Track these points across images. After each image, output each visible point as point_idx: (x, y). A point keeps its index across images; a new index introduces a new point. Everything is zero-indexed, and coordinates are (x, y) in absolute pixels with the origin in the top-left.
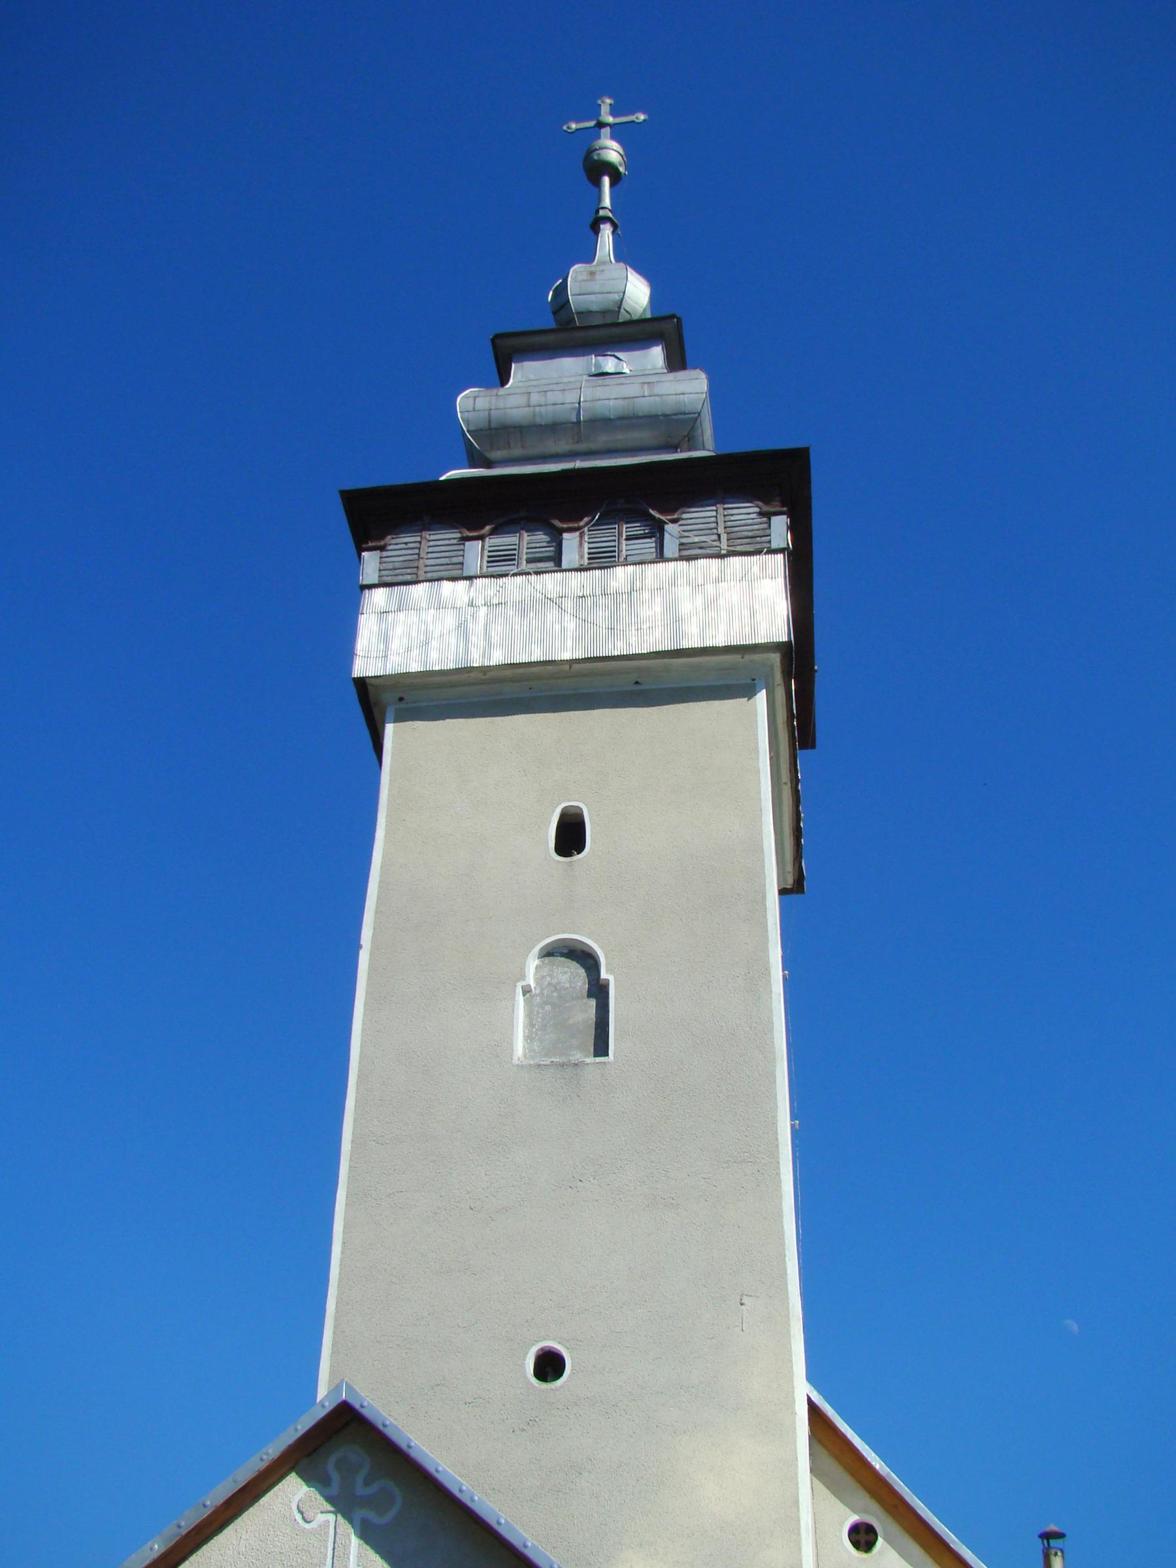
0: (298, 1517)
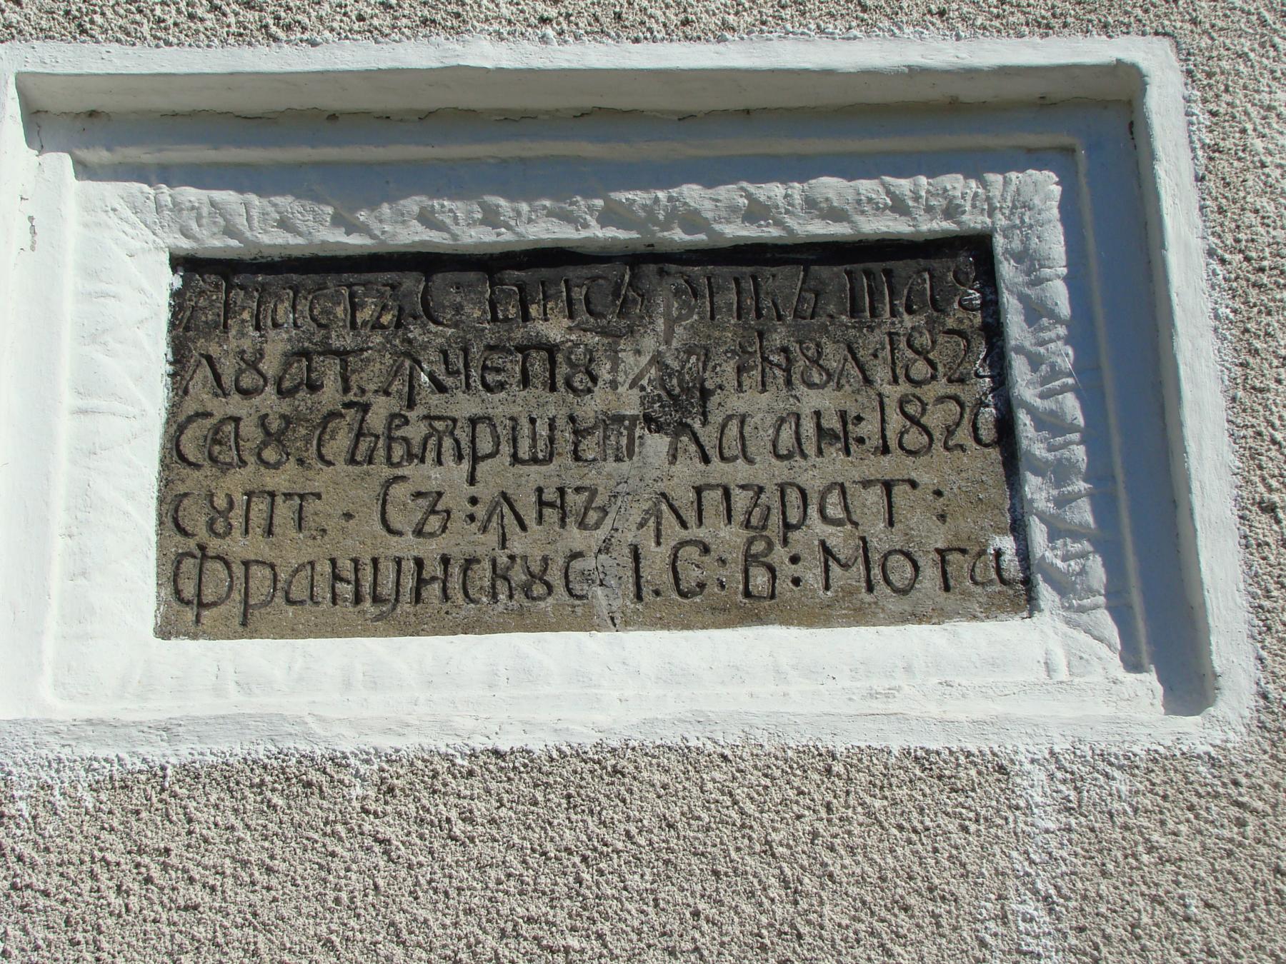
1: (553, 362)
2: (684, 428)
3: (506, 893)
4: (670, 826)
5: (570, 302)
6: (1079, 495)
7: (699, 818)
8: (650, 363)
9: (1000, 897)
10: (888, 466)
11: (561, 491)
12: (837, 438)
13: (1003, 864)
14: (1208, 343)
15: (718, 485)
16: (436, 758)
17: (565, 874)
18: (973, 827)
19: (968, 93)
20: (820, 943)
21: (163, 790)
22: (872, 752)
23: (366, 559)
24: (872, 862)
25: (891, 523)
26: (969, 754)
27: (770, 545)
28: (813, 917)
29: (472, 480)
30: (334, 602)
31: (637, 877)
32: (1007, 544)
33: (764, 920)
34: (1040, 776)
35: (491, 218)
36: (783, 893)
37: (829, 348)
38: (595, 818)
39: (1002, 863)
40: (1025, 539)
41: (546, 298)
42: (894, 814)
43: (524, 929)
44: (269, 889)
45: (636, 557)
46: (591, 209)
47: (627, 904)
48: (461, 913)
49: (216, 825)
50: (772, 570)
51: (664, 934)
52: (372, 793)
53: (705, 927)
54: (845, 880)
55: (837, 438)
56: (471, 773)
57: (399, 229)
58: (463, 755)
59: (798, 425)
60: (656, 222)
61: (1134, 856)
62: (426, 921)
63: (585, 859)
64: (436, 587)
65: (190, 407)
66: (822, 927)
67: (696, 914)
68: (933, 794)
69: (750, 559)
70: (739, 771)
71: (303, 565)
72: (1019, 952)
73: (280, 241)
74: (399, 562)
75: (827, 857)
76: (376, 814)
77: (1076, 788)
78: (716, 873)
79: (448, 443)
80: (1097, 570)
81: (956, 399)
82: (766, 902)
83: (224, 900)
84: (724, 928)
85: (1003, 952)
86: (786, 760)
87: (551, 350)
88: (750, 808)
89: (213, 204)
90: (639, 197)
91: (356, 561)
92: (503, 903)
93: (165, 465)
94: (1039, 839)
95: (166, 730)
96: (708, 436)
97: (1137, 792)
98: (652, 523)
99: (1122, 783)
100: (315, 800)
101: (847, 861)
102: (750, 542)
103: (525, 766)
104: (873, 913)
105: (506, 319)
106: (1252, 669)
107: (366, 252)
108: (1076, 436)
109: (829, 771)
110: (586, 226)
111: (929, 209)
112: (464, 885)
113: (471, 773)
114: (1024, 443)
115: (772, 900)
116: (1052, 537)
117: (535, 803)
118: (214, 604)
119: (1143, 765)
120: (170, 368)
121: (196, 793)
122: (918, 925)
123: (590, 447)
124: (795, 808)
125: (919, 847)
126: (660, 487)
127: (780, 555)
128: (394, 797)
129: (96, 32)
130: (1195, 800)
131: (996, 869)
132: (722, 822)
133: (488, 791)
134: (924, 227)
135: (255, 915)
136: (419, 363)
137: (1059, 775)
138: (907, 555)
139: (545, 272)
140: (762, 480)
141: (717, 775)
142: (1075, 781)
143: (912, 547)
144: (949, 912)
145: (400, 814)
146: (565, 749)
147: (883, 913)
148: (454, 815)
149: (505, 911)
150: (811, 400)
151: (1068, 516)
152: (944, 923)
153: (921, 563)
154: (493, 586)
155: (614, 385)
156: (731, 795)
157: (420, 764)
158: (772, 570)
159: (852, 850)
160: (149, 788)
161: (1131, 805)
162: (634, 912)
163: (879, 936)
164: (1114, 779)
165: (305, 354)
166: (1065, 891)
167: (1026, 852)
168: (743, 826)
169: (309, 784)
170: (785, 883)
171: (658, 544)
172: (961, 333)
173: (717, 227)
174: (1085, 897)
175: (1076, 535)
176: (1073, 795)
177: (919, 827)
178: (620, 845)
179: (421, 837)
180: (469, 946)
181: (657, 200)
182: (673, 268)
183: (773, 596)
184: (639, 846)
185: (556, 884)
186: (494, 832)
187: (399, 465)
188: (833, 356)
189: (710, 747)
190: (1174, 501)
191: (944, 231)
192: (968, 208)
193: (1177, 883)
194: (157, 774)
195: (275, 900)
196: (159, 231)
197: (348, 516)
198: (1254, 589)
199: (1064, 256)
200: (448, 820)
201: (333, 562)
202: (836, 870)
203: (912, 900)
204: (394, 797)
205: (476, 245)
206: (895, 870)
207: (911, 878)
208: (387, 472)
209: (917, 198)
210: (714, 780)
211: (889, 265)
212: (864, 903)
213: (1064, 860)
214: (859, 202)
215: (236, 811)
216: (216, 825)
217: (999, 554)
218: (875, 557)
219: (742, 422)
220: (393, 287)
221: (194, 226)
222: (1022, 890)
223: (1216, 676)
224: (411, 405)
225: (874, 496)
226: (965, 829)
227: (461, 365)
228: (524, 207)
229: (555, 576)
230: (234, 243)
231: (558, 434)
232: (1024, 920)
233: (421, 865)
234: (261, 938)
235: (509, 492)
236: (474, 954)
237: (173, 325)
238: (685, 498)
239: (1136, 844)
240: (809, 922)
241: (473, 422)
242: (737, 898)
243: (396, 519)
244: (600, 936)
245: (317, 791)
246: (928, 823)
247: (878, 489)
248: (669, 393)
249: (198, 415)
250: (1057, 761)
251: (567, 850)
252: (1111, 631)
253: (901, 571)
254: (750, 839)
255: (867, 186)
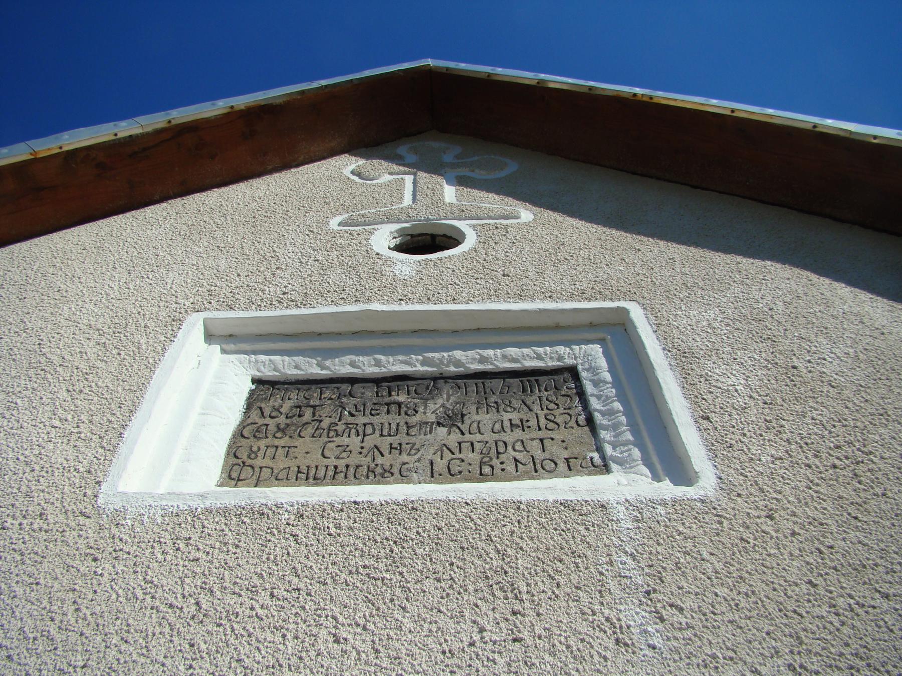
0: (356, 178)
1: (400, 407)
2: (454, 425)
3: (355, 556)
4: (439, 529)
5: (408, 391)
6: (624, 431)
7: (454, 526)
8: (440, 407)
9: (608, 555)
10: (541, 434)
11: (400, 444)
12: (519, 427)
13: (607, 542)
14: (669, 373)
15: (468, 442)
16: (326, 505)
17: (385, 549)
18: (591, 529)
19: (563, 321)
20: (517, 575)
21: (194, 517)
22: (539, 502)
23: (314, 466)
24: (542, 542)
25: (544, 451)
26: (587, 501)
27: (491, 459)
28: (513, 565)
29: (362, 442)
30: (296, 480)
31: (422, 550)
32: (596, 455)
33: (487, 566)
34: (621, 508)
35: (378, 364)
36: (497, 556)
37: (514, 401)
38: (402, 527)
39: (607, 542)
40: (603, 452)
41: (398, 390)
42: (552, 524)
43: (361, 570)
44: (235, 553)
45: (432, 464)
46: (417, 360)
47: (416, 561)
48: (330, 565)
49: (216, 529)
50: (492, 467)
51: (435, 573)
52: (293, 517)
53: (456, 570)
54: (528, 550)
55: (519, 427)
56: (342, 510)
57: (341, 368)
58: (338, 503)
59: (502, 423)
60: (443, 364)
61: (672, 537)
62: (311, 567)
63: (395, 542)
64: (342, 475)
65: (249, 421)
66: (517, 568)
67: (452, 564)
68: (570, 517)
69: (482, 463)
70: (475, 508)
71: (286, 468)
72: (620, 576)
73: (295, 373)
74: (327, 467)
75: (520, 541)
76: (293, 525)
77: (640, 513)
78: (462, 548)
79: (353, 431)
80: (636, 453)
81: (568, 414)
82: (488, 560)
83: (212, 557)
84: (466, 570)
85: (612, 577)
86: (497, 505)
87: (399, 404)
88: (479, 522)
89: (270, 360)
90: (436, 355)
91: (308, 467)
92: (352, 560)
93: (234, 436)
94: (624, 532)
95: (202, 496)
96: (464, 428)
97: (669, 513)
98: (439, 453)
99: (661, 510)
100: (265, 520)
101: (529, 542)
102: (482, 458)
103: (368, 507)
104: (543, 563)
105: (382, 396)
106: (712, 470)
107: (328, 377)
108: (621, 414)
109: (519, 508)
110: (415, 366)
111: (551, 358)
112: (333, 553)
113: (342, 510)
114: (598, 422)
115: (491, 559)
116: (614, 448)
117: (372, 521)
118: (244, 480)
119: (669, 503)
120: (244, 410)
121: (209, 518)
122: (567, 568)
123: (413, 431)
124: (502, 523)
125: (565, 536)
126: (443, 442)
127: (495, 462)
128: (303, 519)
129: (236, 309)
130: (697, 515)
131: (605, 544)
132: (465, 528)
133: (349, 517)
134: (550, 364)
135: (226, 564)
136: (345, 408)
137: (631, 508)
138: (552, 460)
139: (399, 383)
140: (487, 439)
141: (463, 510)
142: (638, 509)
143: (554, 458)
144: (583, 562)
145: (305, 526)
146: (388, 500)
147: (549, 562)
148: (331, 526)
149: (352, 563)
150: (506, 416)
151: (620, 439)
152: (580, 565)
153: (558, 462)
154: (368, 474)
155: (425, 413)
156: (470, 517)
157: (317, 507)
158: (492, 467)
159: (532, 538)
160: (188, 516)
161: (667, 518)
162: (419, 564)
163: (547, 571)
164: (657, 508)
165: (299, 407)
166: (640, 551)
167: (619, 537)
168: (476, 529)
169: (263, 514)
170: (498, 552)
171: (442, 459)
172: (568, 396)
173: (467, 365)
174: (651, 553)
175: (625, 444)
176: (639, 515)
177: (565, 529)
178: (413, 537)
179: (314, 534)
180: (332, 577)
181: (443, 356)
182: (450, 381)
183: (493, 475)
184: (423, 537)
185: (380, 552)
186: (351, 532)
187: (332, 437)
188: (516, 404)
189: (460, 500)
190: (665, 427)
191: (558, 365)
192: (566, 357)
193: (695, 546)
194: (192, 512)
195: (237, 558)
196: (248, 369)
197: (307, 453)
198: (706, 443)
199: (607, 366)
200: (328, 528)
201: (298, 467)
202: (524, 546)
203: (564, 557)
204: (303, 519)
205: (371, 374)
206: (554, 546)
207: (562, 548)
208: (327, 440)
209: (546, 354)
210: (461, 512)
211: (537, 378)
212: (539, 559)
213: (638, 540)
214: (523, 356)
215: (226, 524)
216: (216, 529)
217: (592, 458)
218: (538, 462)
219: (479, 423)
220: (338, 388)
221: (262, 368)
222: (619, 552)
223: (697, 473)
224: (340, 420)
225: (536, 443)
226: (587, 529)
227: (362, 409)
228: (391, 359)
229: (395, 470)
230: (277, 374)
231: (400, 427)
232: (621, 564)
233: (312, 545)
234: (226, 572)
235: (378, 445)
236: (335, 580)
237: (248, 399)
238: (454, 446)
239: (672, 532)
240: (511, 567)
241: (365, 425)
242: (473, 558)
243: (327, 453)
244: (401, 574)
245: (266, 517)
246: (568, 526)
247: (538, 441)
248: (448, 416)
249: (252, 423)
250: (629, 502)
251: (386, 538)
252: (646, 471)
253: (549, 465)
254: (480, 534)
255: (526, 351)
